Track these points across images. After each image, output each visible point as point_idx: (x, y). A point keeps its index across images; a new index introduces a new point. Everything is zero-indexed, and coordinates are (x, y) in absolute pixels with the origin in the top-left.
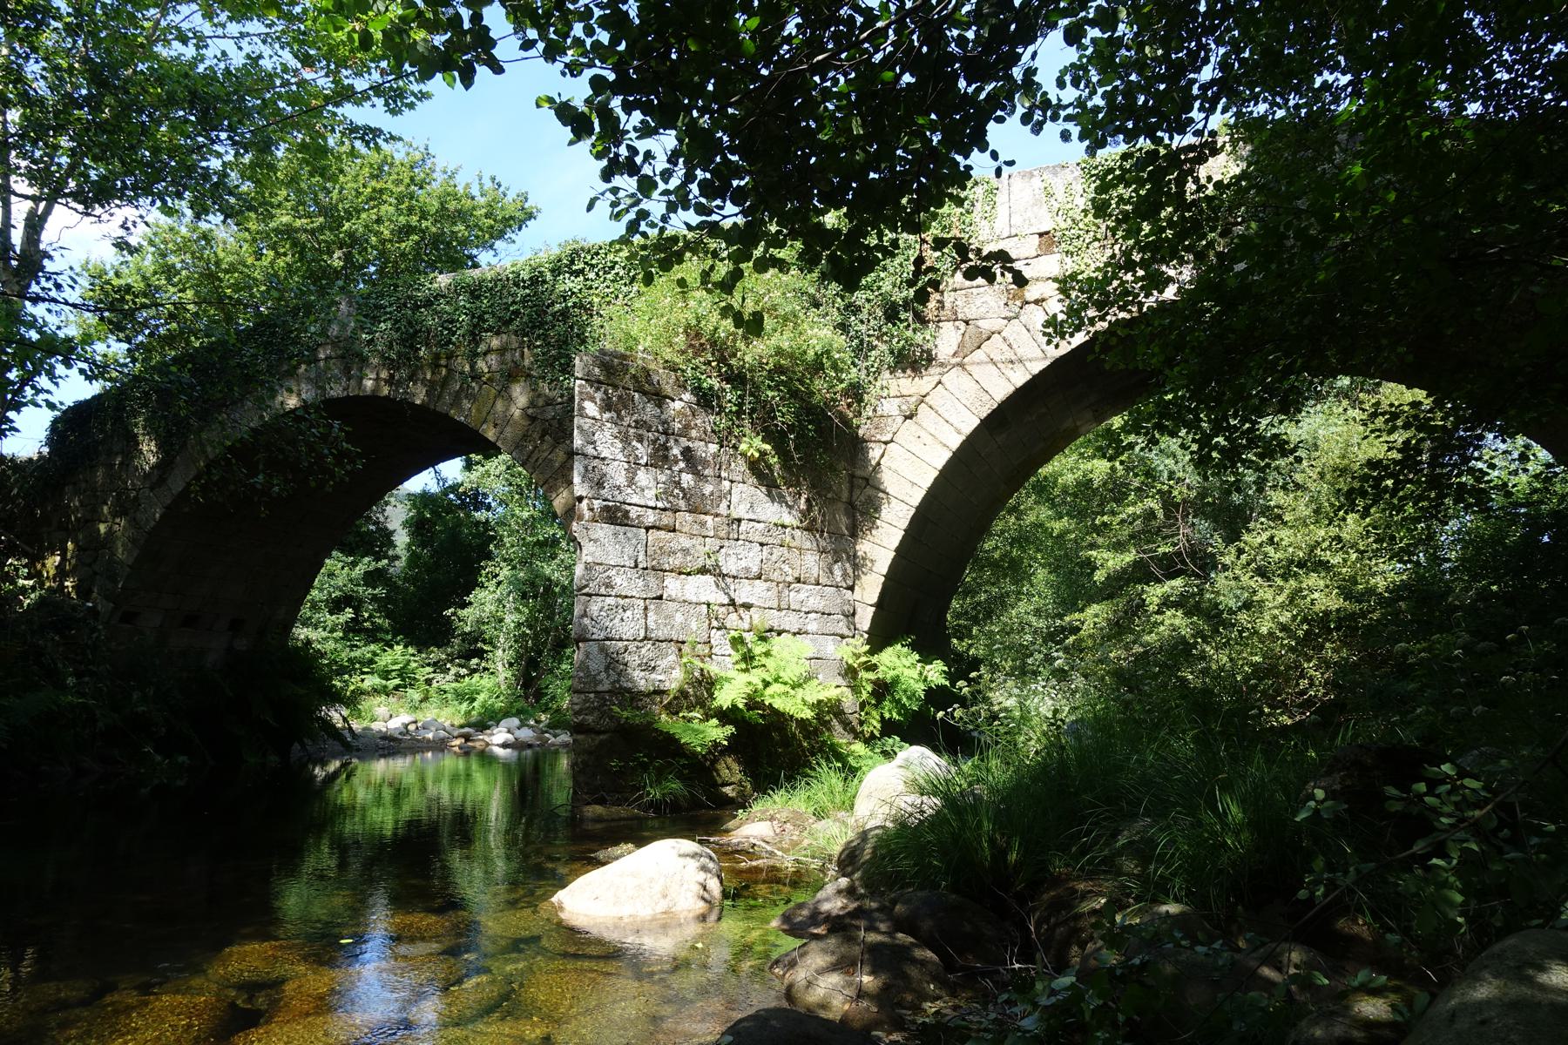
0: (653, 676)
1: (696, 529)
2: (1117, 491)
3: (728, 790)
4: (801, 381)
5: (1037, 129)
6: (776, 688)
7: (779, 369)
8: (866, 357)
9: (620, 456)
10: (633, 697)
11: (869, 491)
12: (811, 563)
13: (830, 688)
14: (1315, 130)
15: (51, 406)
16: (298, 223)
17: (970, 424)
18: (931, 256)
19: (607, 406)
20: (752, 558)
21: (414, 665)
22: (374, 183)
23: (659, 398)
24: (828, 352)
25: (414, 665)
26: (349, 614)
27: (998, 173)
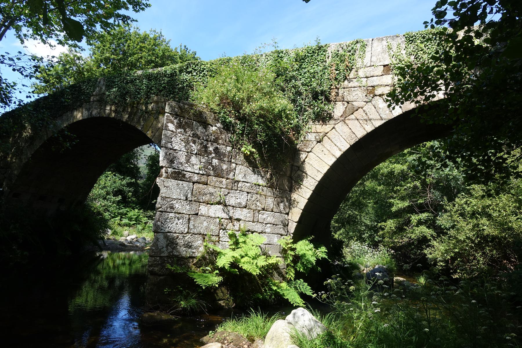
0: (190, 250)
3: (221, 302)
4: (270, 122)
6: (246, 259)
7: (261, 116)
9: (183, 149)
11: (300, 173)
12: (270, 202)
19: (179, 126)
20: (243, 199)
21: (141, 216)
22: (141, 44)
23: (205, 124)
24: (284, 110)
25: (141, 216)
26: (119, 198)
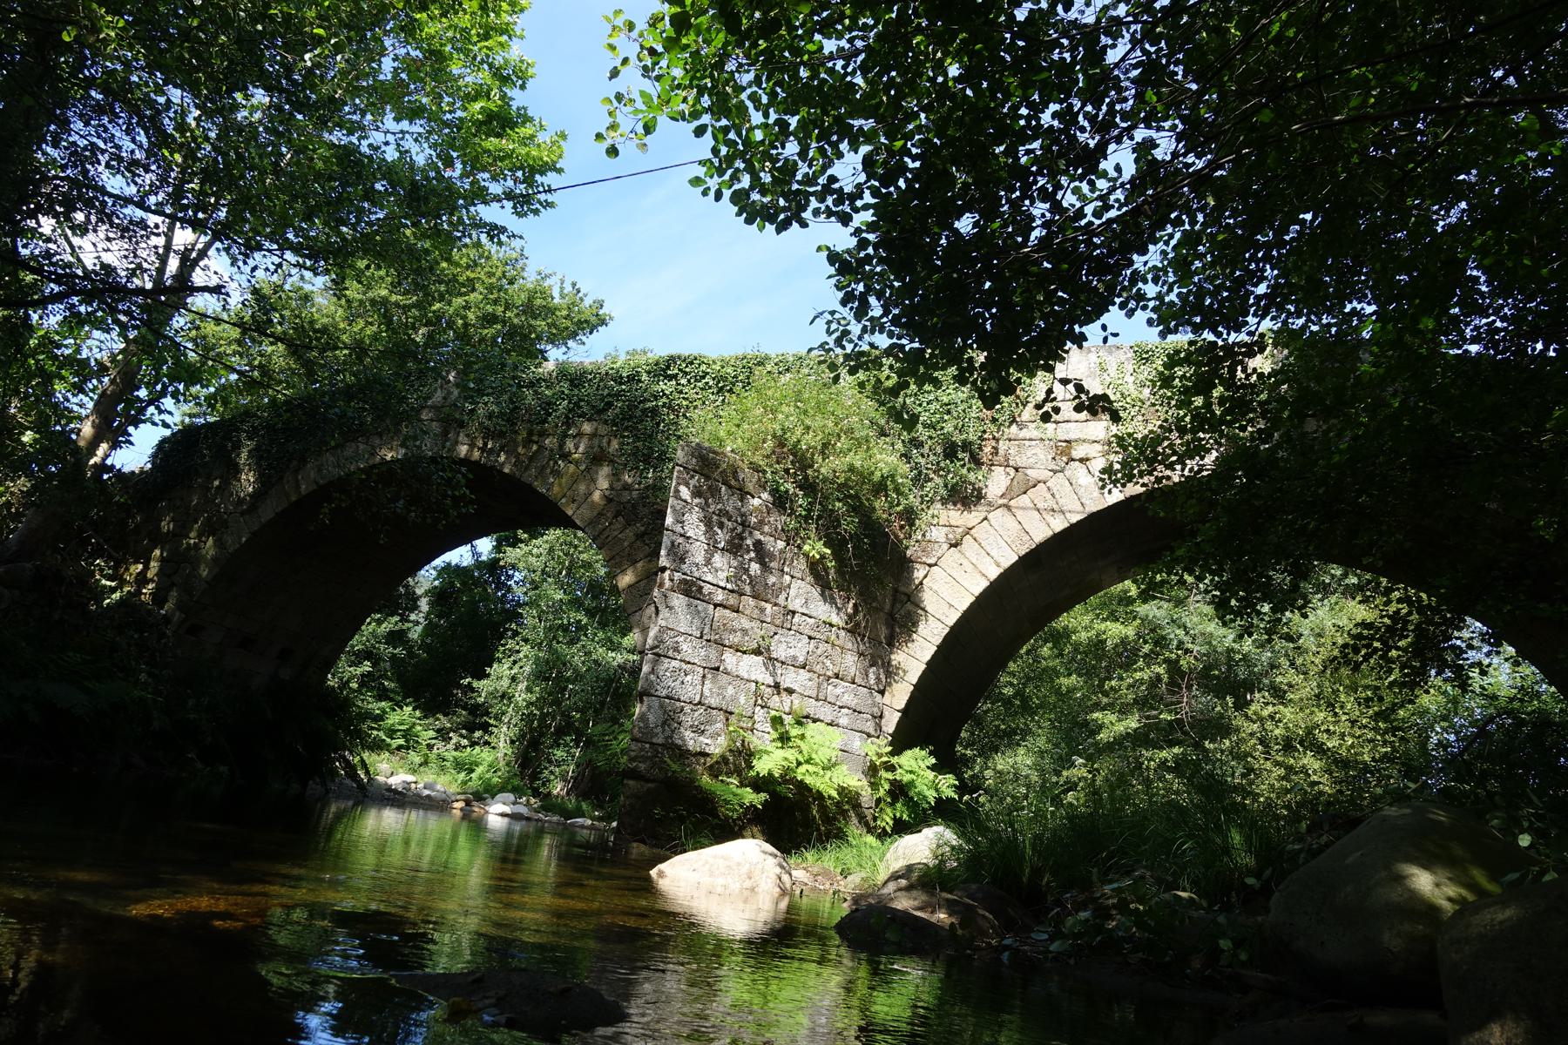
1: (756, 613)
2: (1126, 656)
5: (1130, 314)
8: (922, 487)
10: (682, 753)
11: (909, 606)
12: (850, 663)
13: (855, 781)
14: (1342, 346)
15: (166, 425)
16: (394, 298)
17: (1010, 559)
18: (1058, 389)
19: (697, 493)
23: (743, 494)
26: (367, 667)
27: (1105, 340)
